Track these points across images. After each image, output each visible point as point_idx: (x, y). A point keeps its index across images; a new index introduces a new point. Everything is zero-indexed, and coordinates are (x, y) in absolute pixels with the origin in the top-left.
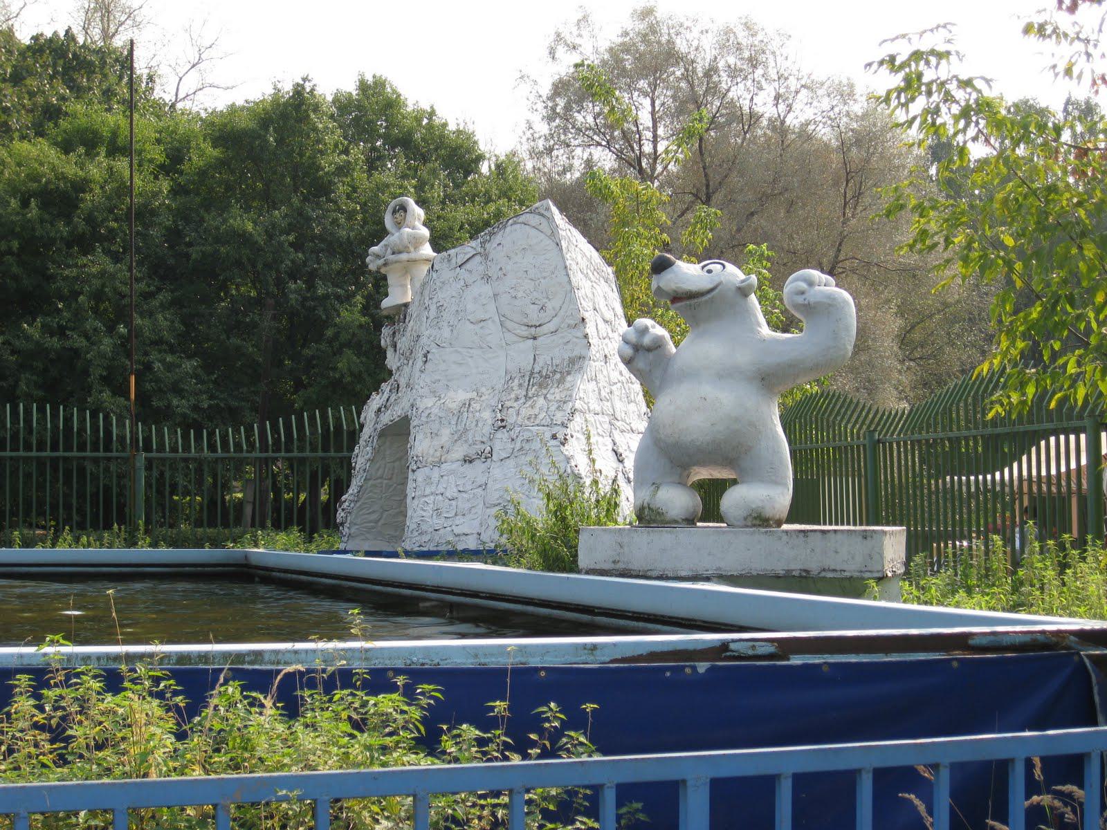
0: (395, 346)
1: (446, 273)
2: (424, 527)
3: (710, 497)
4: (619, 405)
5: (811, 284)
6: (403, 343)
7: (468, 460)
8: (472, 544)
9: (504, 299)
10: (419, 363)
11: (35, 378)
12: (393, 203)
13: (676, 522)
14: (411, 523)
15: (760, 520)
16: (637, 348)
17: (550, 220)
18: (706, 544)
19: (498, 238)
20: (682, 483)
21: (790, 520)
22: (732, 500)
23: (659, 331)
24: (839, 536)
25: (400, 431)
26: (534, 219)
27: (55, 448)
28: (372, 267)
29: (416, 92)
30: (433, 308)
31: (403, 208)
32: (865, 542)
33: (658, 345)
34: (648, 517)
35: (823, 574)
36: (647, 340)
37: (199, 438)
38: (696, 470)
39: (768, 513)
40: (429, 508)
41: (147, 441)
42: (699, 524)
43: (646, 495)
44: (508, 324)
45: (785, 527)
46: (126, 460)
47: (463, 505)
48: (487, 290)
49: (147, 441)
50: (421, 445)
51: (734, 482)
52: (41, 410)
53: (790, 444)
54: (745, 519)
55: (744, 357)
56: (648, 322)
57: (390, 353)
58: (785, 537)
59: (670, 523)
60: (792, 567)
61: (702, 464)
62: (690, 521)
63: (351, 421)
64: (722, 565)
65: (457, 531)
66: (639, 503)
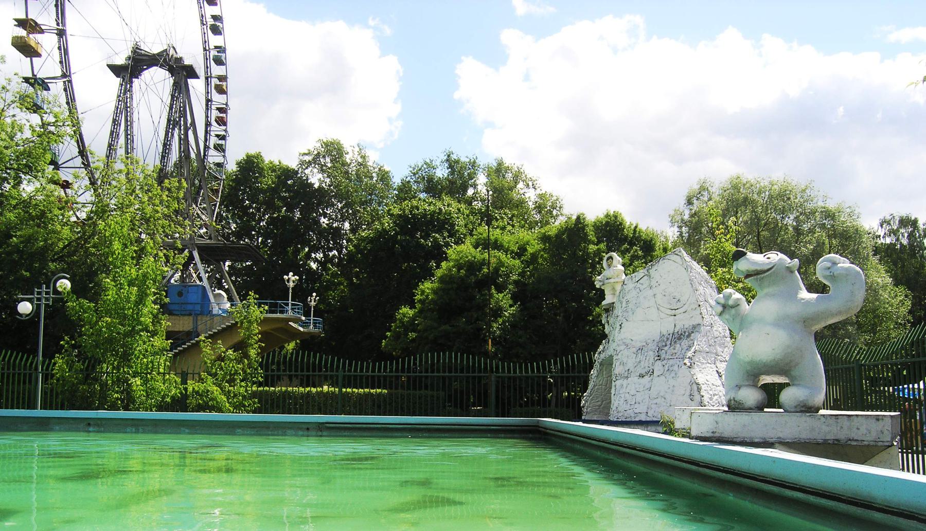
0: (608, 322)
1: (630, 285)
2: (619, 409)
3: (771, 395)
4: (719, 349)
5: (835, 263)
6: (611, 320)
7: (641, 376)
8: (643, 418)
9: (659, 296)
10: (618, 329)
11: (61, 245)
12: (607, 256)
13: (751, 409)
14: (613, 407)
15: (808, 409)
16: (724, 307)
17: (682, 257)
18: (770, 421)
19: (655, 268)
20: (755, 386)
21: (825, 406)
22: (786, 396)
23: (738, 295)
24: (860, 418)
25: (608, 363)
26: (674, 257)
27: (450, 372)
28: (598, 286)
29: (630, 219)
30: (624, 303)
31: (611, 258)
32: (878, 423)
33: (736, 305)
34: (734, 407)
35: (849, 442)
36: (731, 302)
37: (520, 368)
38: (766, 388)
39: (810, 403)
40: (622, 400)
41: (497, 368)
42: (766, 410)
43: (732, 395)
44: (661, 308)
45: (822, 412)
46: (487, 377)
47: (639, 399)
48: (650, 293)
49: (497, 368)
50: (618, 369)
51: (788, 385)
52: (462, 356)
53: (824, 366)
54: (796, 407)
55: (792, 309)
56: (729, 290)
57: (606, 326)
58: (822, 418)
59: (749, 410)
60: (828, 438)
61: (768, 373)
62: (760, 408)
63: (591, 359)
64: (781, 435)
65: (636, 411)
66: (728, 397)
